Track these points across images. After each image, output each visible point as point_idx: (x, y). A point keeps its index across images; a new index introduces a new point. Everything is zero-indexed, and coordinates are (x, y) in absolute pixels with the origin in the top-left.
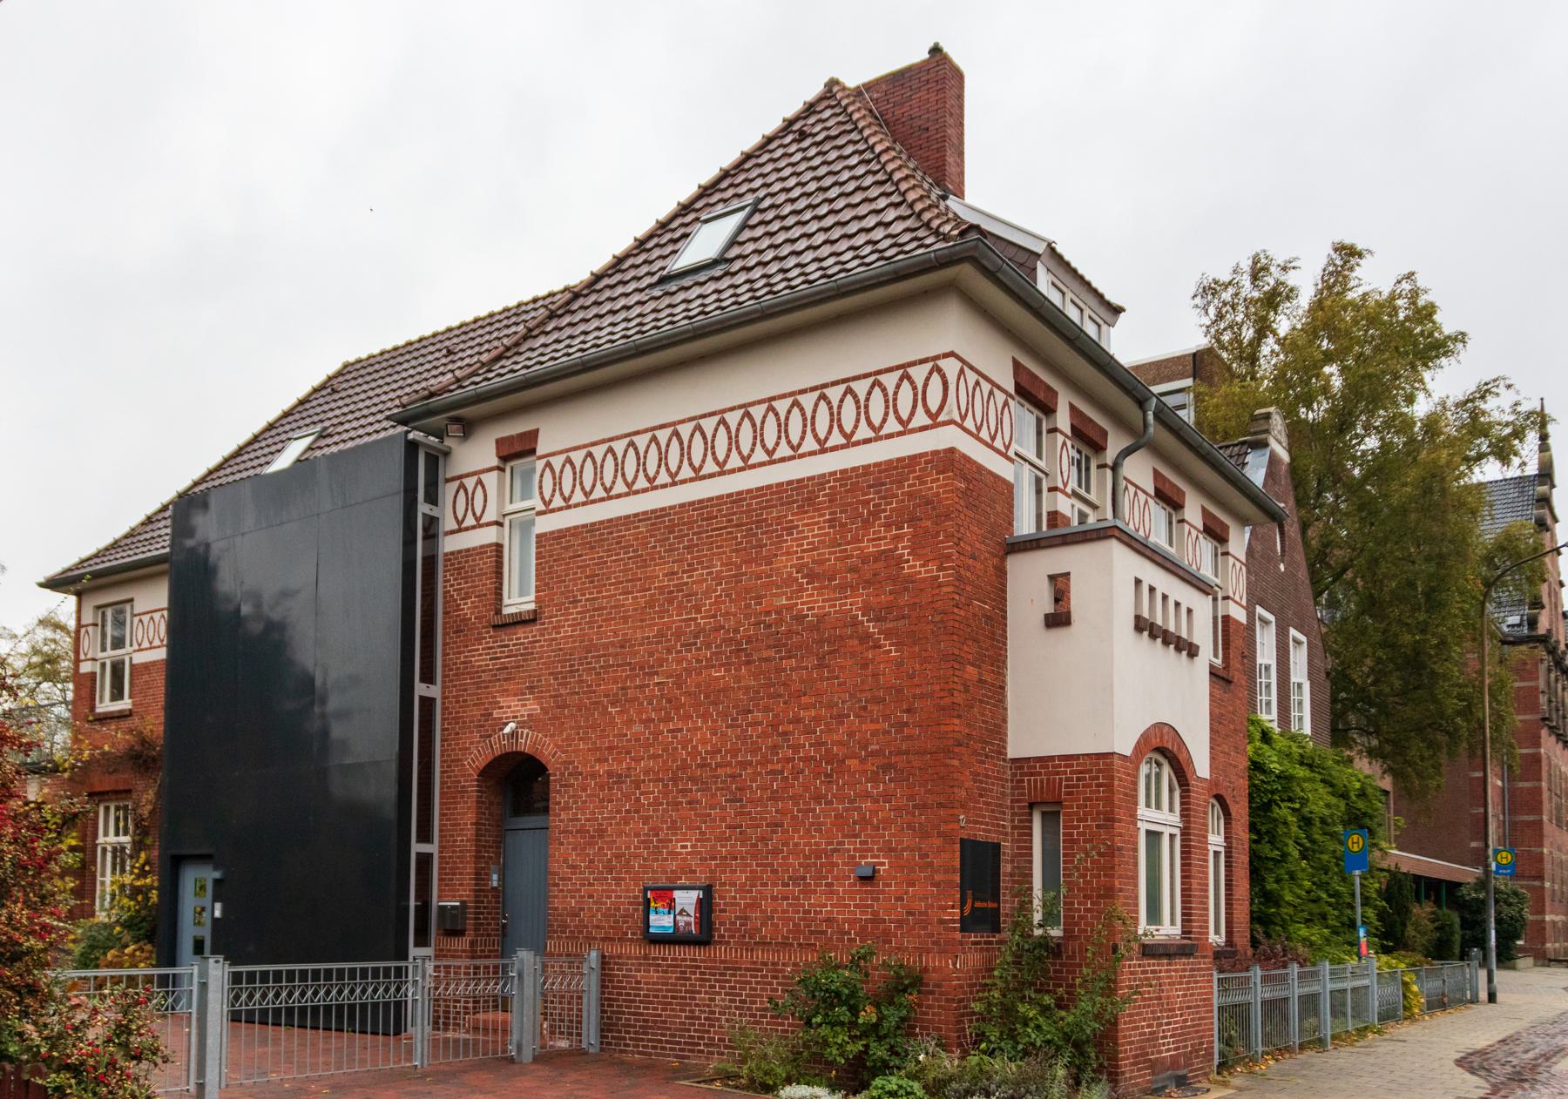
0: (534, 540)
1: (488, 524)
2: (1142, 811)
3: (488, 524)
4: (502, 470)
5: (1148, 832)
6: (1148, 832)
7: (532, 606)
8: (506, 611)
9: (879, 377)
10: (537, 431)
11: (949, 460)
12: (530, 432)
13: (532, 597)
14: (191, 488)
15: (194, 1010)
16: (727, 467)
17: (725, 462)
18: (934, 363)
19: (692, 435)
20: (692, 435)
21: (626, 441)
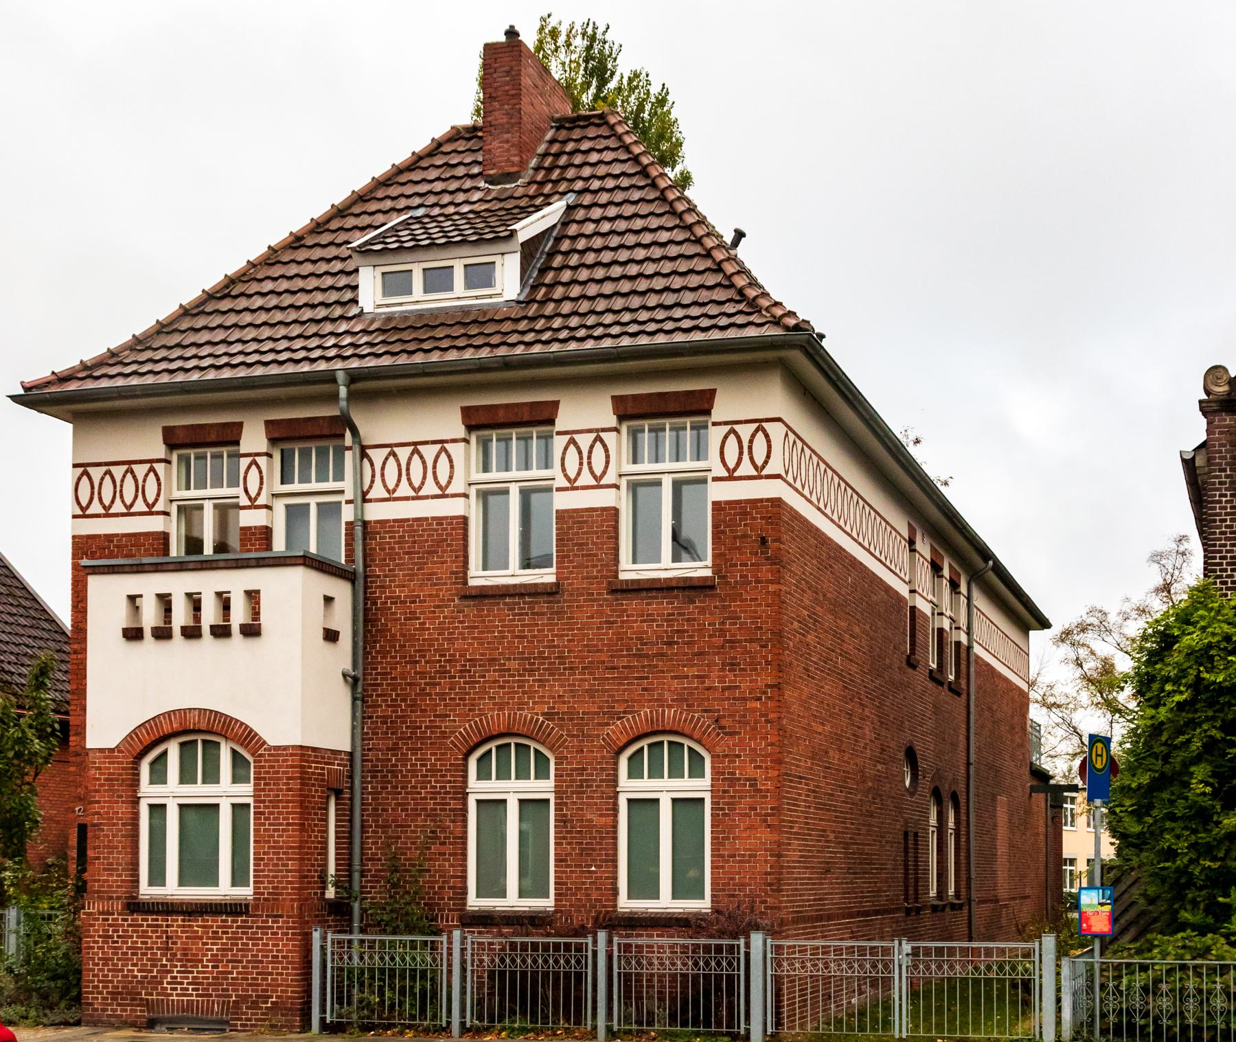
0: (343, 526)
1: (158, 513)
2: (624, 781)
3: (158, 513)
4: (466, 441)
5: (151, 806)
6: (151, 806)
7: (708, 573)
8: (472, 583)
9: (575, 436)
10: (715, 390)
11: (777, 503)
12: (553, 402)
13: (709, 562)
14: (48, 383)
15: (742, 973)
16: (111, 511)
17: (110, 506)
18: (760, 424)
19: (124, 476)
20: (124, 476)
21: (104, 469)
